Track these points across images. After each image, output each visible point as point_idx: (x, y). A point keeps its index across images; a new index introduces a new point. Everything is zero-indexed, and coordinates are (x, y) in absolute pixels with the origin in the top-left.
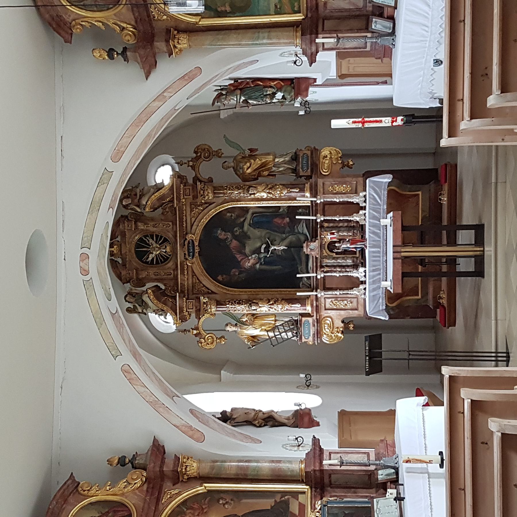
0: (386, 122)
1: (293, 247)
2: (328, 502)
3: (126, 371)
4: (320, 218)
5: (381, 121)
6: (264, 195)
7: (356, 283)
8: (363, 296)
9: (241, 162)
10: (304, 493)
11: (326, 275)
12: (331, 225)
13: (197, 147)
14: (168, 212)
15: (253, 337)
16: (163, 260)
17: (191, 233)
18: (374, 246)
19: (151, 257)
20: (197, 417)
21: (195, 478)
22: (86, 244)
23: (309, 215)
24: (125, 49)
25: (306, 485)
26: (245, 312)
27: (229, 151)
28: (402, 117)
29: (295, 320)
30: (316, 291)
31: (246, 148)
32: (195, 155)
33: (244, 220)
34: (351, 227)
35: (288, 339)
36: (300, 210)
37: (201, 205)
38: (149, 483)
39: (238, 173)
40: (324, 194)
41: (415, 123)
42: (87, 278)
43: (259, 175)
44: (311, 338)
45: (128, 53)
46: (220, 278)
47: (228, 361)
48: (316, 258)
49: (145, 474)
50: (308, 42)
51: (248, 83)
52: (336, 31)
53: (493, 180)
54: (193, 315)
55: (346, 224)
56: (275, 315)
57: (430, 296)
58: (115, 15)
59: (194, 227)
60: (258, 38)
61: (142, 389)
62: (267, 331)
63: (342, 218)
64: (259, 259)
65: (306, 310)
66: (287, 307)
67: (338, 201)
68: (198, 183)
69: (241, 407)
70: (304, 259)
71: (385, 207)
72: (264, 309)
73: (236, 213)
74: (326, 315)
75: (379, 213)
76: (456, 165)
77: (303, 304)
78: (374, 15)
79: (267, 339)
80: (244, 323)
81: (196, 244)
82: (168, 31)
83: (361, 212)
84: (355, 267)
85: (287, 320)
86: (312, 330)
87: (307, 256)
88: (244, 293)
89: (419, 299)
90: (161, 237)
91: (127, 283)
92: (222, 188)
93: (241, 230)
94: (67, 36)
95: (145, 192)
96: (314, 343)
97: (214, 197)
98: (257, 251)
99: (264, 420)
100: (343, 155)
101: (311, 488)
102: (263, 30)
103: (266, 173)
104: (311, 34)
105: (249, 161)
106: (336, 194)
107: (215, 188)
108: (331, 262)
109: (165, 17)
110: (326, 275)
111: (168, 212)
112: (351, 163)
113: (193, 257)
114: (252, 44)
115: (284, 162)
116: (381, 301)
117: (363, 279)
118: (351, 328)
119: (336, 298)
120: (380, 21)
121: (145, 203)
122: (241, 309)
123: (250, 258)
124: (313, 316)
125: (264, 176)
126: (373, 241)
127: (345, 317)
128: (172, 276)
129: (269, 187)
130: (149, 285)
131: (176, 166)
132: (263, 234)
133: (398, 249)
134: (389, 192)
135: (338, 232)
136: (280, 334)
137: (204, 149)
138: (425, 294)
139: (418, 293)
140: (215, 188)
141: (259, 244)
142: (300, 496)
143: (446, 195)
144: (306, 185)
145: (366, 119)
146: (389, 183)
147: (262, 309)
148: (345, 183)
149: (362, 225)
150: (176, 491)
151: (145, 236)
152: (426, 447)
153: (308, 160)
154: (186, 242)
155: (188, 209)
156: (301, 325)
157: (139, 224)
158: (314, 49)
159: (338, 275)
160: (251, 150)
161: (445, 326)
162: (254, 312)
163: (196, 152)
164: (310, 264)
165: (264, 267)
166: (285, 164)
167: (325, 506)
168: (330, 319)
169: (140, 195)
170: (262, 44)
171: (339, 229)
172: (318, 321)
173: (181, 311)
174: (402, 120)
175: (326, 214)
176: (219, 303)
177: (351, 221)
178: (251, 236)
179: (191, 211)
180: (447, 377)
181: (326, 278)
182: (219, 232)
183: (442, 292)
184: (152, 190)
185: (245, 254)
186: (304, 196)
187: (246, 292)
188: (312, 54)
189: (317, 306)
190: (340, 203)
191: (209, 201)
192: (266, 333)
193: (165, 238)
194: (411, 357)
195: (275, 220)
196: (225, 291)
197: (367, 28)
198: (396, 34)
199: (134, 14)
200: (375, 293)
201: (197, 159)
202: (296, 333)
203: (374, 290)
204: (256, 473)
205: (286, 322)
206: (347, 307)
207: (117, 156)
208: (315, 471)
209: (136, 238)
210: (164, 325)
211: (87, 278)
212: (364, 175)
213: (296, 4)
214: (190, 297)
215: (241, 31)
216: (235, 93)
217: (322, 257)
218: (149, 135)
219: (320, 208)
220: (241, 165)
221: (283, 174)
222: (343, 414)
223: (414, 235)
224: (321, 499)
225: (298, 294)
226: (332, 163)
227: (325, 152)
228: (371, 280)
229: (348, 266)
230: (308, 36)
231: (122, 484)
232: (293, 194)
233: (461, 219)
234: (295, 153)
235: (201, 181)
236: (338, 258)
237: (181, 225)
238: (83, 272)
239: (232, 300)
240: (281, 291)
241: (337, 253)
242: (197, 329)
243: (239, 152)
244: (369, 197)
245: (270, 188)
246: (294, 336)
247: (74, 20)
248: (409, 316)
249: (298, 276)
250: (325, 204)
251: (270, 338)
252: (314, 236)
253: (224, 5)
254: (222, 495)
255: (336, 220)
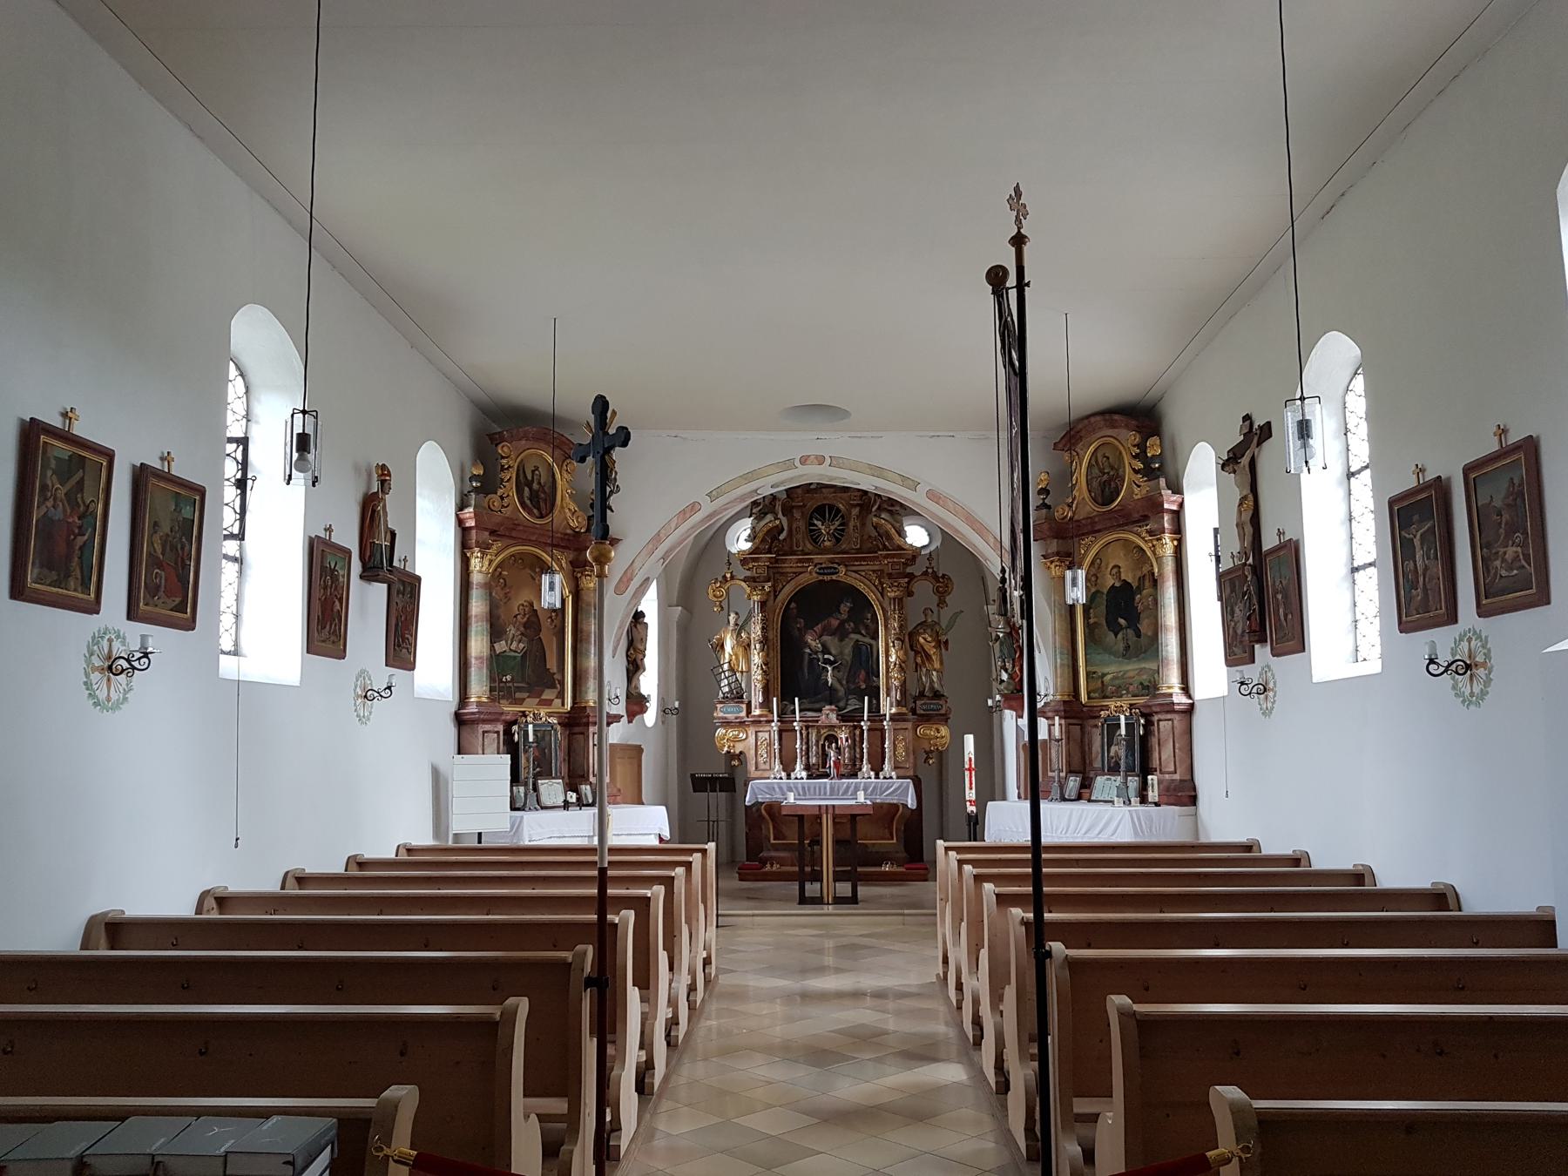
0: (971, 794)
1: (830, 694)
2: (555, 730)
3: (694, 507)
4: (865, 725)
5: (971, 789)
6: (893, 659)
7: (788, 768)
8: (772, 776)
9: (932, 630)
10: (563, 705)
11: (798, 732)
12: (857, 739)
13: (950, 578)
14: (872, 543)
15: (722, 645)
16: (814, 536)
17: (847, 570)
18: (832, 788)
19: (819, 523)
20: (641, 585)
21: (577, 586)
22: (835, 462)
23: (869, 712)
24: (1049, 507)
25: (571, 708)
26: (753, 635)
27: (946, 614)
28: (975, 811)
29: (742, 696)
30: (778, 721)
31: (949, 636)
32: (940, 575)
33: (862, 634)
34: (855, 762)
35: (721, 688)
36: (874, 702)
37: (881, 583)
38: (574, 536)
39: (919, 627)
40: (894, 729)
41: (969, 825)
42: (797, 463)
43: (917, 653)
44: (721, 715)
45: (1044, 511)
46: (793, 605)
47: (691, 613)
48: (817, 721)
49: (582, 531)
50: (1057, 708)
51: (1018, 641)
52: (1068, 738)
53: (906, 911)
54: (748, 574)
55: (858, 756)
56: (749, 671)
57: (773, 854)
58: (1083, 499)
59: (853, 574)
60: (1061, 653)
61: (673, 525)
62: (729, 662)
63: (865, 751)
64: (816, 653)
65: (756, 708)
66: (759, 686)
67: (886, 746)
68: (906, 580)
69: (649, 634)
70: (817, 706)
71: (878, 801)
72: (757, 659)
73: (870, 625)
74: (749, 732)
75: (872, 793)
76: (926, 880)
77: (762, 705)
78: (1083, 779)
79: (719, 662)
80: (739, 634)
81: (834, 577)
82: (1069, 555)
83: (872, 774)
84: (807, 767)
85: (743, 685)
86: (731, 717)
87: (820, 710)
88: (775, 635)
89: (769, 841)
90: (842, 536)
91: (788, 495)
92: (901, 608)
93: (850, 630)
94: (1060, 446)
95: (896, 516)
96: (716, 719)
97: (890, 599)
98: (826, 650)
99: (635, 660)
100: (941, 752)
101: (568, 713)
102: (1070, 658)
103: (919, 660)
104: (1065, 711)
105: (933, 640)
106: (894, 743)
107: (901, 600)
108: (813, 738)
109: (1083, 552)
110: (798, 732)
111: (872, 543)
112: (931, 762)
113: (816, 573)
114: (1055, 647)
115: (932, 682)
116: (768, 796)
117: (793, 776)
118: (733, 763)
119: (770, 745)
120: (1078, 784)
121: (883, 516)
122: (756, 631)
123: (818, 641)
124: (748, 717)
125: (915, 659)
126: (838, 787)
127: (747, 755)
128: (795, 548)
129: (903, 665)
130: (785, 521)
131: (928, 551)
132: (845, 657)
133: (830, 811)
134: (896, 806)
135: (848, 746)
136: (726, 678)
137: (947, 587)
138: (776, 848)
139: (779, 840)
140: (901, 600)
141: (833, 652)
142: (559, 701)
143: (892, 870)
144: (904, 709)
145: (973, 773)
146: (907, 806)
147: (756, 657)
148: (907, 754)
149: (857, 775)
150: (564, 565)
151: (842, 517)
152: (618, 835)
153: (935, 710)
154: (836, 566)
155: (876, 568)
156: (737, 702)
157: (858, 509)
158: (1050, 714)
159: (797, 746)
160: (946, 643)
161: (739, 869)
162: (753, 647)
163: (944, 575)
164: (810, 714)
165: (806, 657)
166: (930, 683)
167: (552, 727)
168: (744, 737)
169: (891, 511)
170: (1056, 659)
171: (852, 747)
172: (742, 724)
173: (754, 560)
174: (972, 811)
175: (871, 732)
176: (763, 604)
177: (862, 761)
178: (844, 643)
179: (874, 571)
180: (706, 847)
181: (794, 733)
182: (848, 604)
183: (778, 866)
184: (898, 525)
185: (821, 636)
186: (891, 706)
187: (777, 636)
188: (1044, 712)
189: (760, 722)
190: (883, 749)
191: (885, 592)
192: (727, 661)
193: (841, 540)
194: (711, 823)
195: (863, 672)
196: (778, 610)
197: (1071, 772)
198: (1063, 802)
199: (1083, 519)
200: (777, 790)
201: (935, 577)
202: (727, 697)
203: (781, 788)
204: (584, 651)
205: (741, 684)
206: (759, 756)
207: (933, 495)
208: (588, 716)
209: (841, 505)
210: (734, 536)
211: (797, 463)
212: (917, 776)
213: (1097, 695)
214: (771, 570)
215: (1069, 635)
216: (1007, 626)
217: (819, 728)
218: (957, 531)
219: (877, 725)
220: (929, 631)
221: (918, 681)
222: (638, 750)
223: (846, 833)
224: (559, 724)
225: (775, 699)
226: (931, 739)
227: (944, 731)
228: (792, 785)
229: (808, 758)
230: (1062, 708)
231: (573, 506)
232: (893, 693)
233: (861, 885)
234: (943, 696)
235: (908, 583)
236: (817, 746)
237: (857, 559)
238: (803, 460)
239: (767, 620)
240: (777, 678)
241: (823, 746)
242: (732, 578)
243: (944, 627)
244: (890, 783)
245: (900, 664)
246: (724, 694)
247: (1078, 454)
248: (750, 830)
249: (796, 699)
250: (883, 731)
251: (721, 666)
252: (843, 718)
253: (1095, 617)
254: (560, 615)
255: (863, 743)
